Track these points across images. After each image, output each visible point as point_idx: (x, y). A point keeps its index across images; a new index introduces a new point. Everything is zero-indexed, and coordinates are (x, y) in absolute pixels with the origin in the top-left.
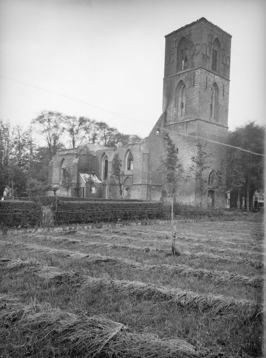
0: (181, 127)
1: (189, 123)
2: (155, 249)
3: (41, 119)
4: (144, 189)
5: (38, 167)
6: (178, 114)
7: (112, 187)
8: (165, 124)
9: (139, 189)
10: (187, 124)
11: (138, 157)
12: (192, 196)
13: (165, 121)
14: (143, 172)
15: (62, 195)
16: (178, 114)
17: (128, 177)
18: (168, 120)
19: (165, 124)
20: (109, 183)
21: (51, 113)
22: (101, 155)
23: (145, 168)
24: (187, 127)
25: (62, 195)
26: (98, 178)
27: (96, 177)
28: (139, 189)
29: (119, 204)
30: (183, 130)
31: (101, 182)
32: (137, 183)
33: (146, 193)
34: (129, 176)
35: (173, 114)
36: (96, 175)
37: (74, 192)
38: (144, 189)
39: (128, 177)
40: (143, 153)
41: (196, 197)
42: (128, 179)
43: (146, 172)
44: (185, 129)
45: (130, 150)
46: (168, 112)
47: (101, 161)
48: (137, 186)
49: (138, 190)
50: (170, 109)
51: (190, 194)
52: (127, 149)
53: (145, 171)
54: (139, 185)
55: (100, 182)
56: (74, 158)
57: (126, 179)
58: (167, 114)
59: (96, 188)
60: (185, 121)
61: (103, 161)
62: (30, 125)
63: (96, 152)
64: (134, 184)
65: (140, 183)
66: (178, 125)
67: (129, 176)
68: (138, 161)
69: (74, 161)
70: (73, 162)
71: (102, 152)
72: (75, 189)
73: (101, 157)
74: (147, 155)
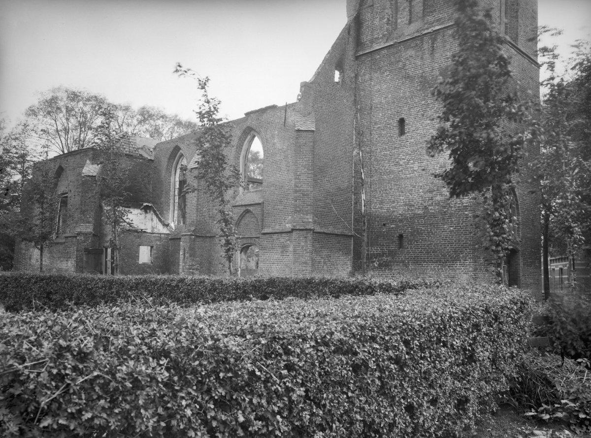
0: (411, 52)
1: (439, 39)
2: (304, 363)
3: (51, 106)
4: (303, 244)
5: (356, 270)
6: (399, 21)
7: (199, 242)
8: (357, 51)
9: (284, 248)
10: (434, 40)
11: (278, 146)
12: (463, 265)
13: (359, 43)
14: (296, 192)
15: (54, 270)
16: (396, 20)
17: (247, 211)
18: (366, 38)
19: (357, 51)
20: (189, 231)
21: (74, 96)
22: (168, 156)
23: (303, 177)
24: (433, 50)
25: (54, 270)
26: (160, 220)
27: (155, 218)
28: (284, 248)
29: (223, 360)
30: (419, 63)
31: (168, 232)
32: (278, 228)
33: (307, 257)
34: (251, 208)
35: (382, 18)
36: (155, 212)
37: (84, 259)
38: (303, 244)
39: (247, 211)
40: (299, 131)
41: (475, 270)
42: (248, 219)
43: (307, 191)
44: (427, 56)
45: (254, 127)
46: (367, 16)
47: (169, 171)
48: (275, 236)
49: (280, 250)
50: (372, 6)
51: (455, 259)
52: (245, 126)
53: (305, 187)
54: (284, 235)
55: (165, 231)
56: (88, 162)
57: (242, 216)
58: (362, 23)
59: (152, 247)
60: (426, 32)
61: (173, 172)
62: (23, 119)
63: (154, 149)
64: (266, 231)
65: (289, 226)
66: (402, 47)
67: (251, 208)
68: (278, 158)
69: (87, 169)
70: (84, 171)
71: (173, 145)
72: (86, 250)
73: (166, 160)
74: (310, 135)
